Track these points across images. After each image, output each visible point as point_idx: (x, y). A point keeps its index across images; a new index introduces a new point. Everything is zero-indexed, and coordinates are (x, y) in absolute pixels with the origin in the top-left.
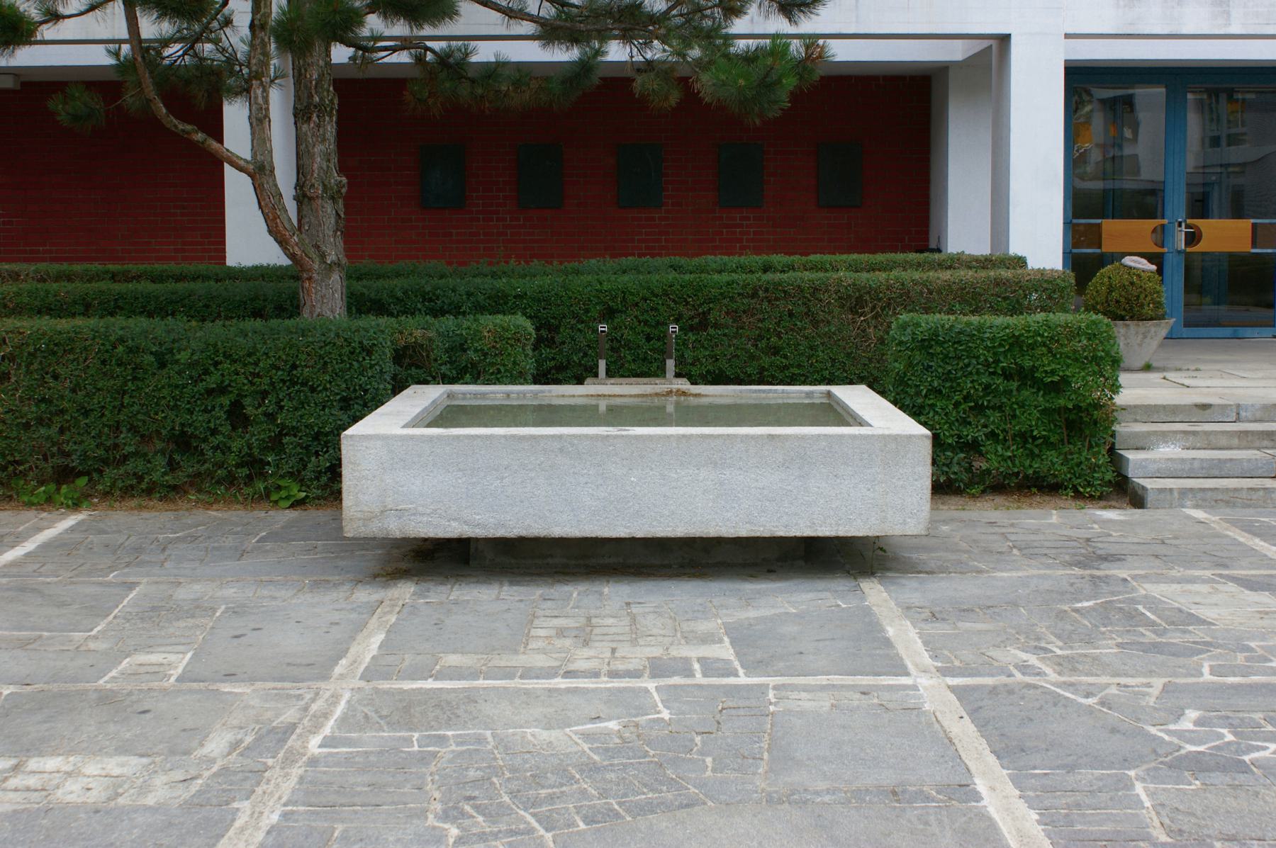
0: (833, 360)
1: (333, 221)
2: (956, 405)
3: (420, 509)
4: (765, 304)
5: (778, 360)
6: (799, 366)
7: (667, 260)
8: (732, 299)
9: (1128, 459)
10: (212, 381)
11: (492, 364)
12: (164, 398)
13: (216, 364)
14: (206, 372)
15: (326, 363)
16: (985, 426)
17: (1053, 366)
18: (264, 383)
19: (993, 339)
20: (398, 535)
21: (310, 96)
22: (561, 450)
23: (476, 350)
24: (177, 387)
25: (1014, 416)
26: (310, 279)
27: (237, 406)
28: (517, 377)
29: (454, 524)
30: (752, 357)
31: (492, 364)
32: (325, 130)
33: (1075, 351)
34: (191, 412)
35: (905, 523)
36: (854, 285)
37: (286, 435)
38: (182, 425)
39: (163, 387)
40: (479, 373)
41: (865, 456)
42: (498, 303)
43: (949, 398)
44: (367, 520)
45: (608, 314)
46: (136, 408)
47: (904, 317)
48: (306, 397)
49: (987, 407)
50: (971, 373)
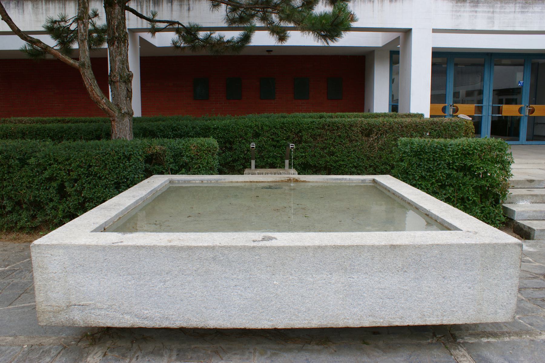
0: (359, 158)
1: (125, 93)
2: (432, 184)
3: (99, 305)
4: (328, 132)
5: (334, 158)
6: (343, 161)
7: (280, 114)
8: (313, 129)
9: (513, 212)
10: (46, 174)
11: (196, 164)
12: (24, 182)
13: (50, 165)
14: (45, 169)
15: (106, 164)
16: (445, 194)
17: (482, 165)
18: (74, 175)
19: (452, 151)
20: (82, 324)
21: (114, 33)
22: (214, 259)
23: (187, 156)
24: (31, 176)
25: (459, 190)
26: (114, 120)
27: (61, 187)
28: (210, 171)
29: (127, 317)
30: (322, 157)
31: (196, 164)
32: (121, 49)
33: (492, 157)
34: (38, 190)
35: (496, 313)
36: (368, 123)
37: (87, 202)
38: (35, 197)
39: (23, 177)
40: (190, 168)
41: (469, 261)
42: (205, 132)
43: (428, 180)
44: (57, 313)
45: (257, 135)
46: (10, 187)
47: (404, 139)
48: (97, 182)
49: (447, 185)
50: (441, 168)
